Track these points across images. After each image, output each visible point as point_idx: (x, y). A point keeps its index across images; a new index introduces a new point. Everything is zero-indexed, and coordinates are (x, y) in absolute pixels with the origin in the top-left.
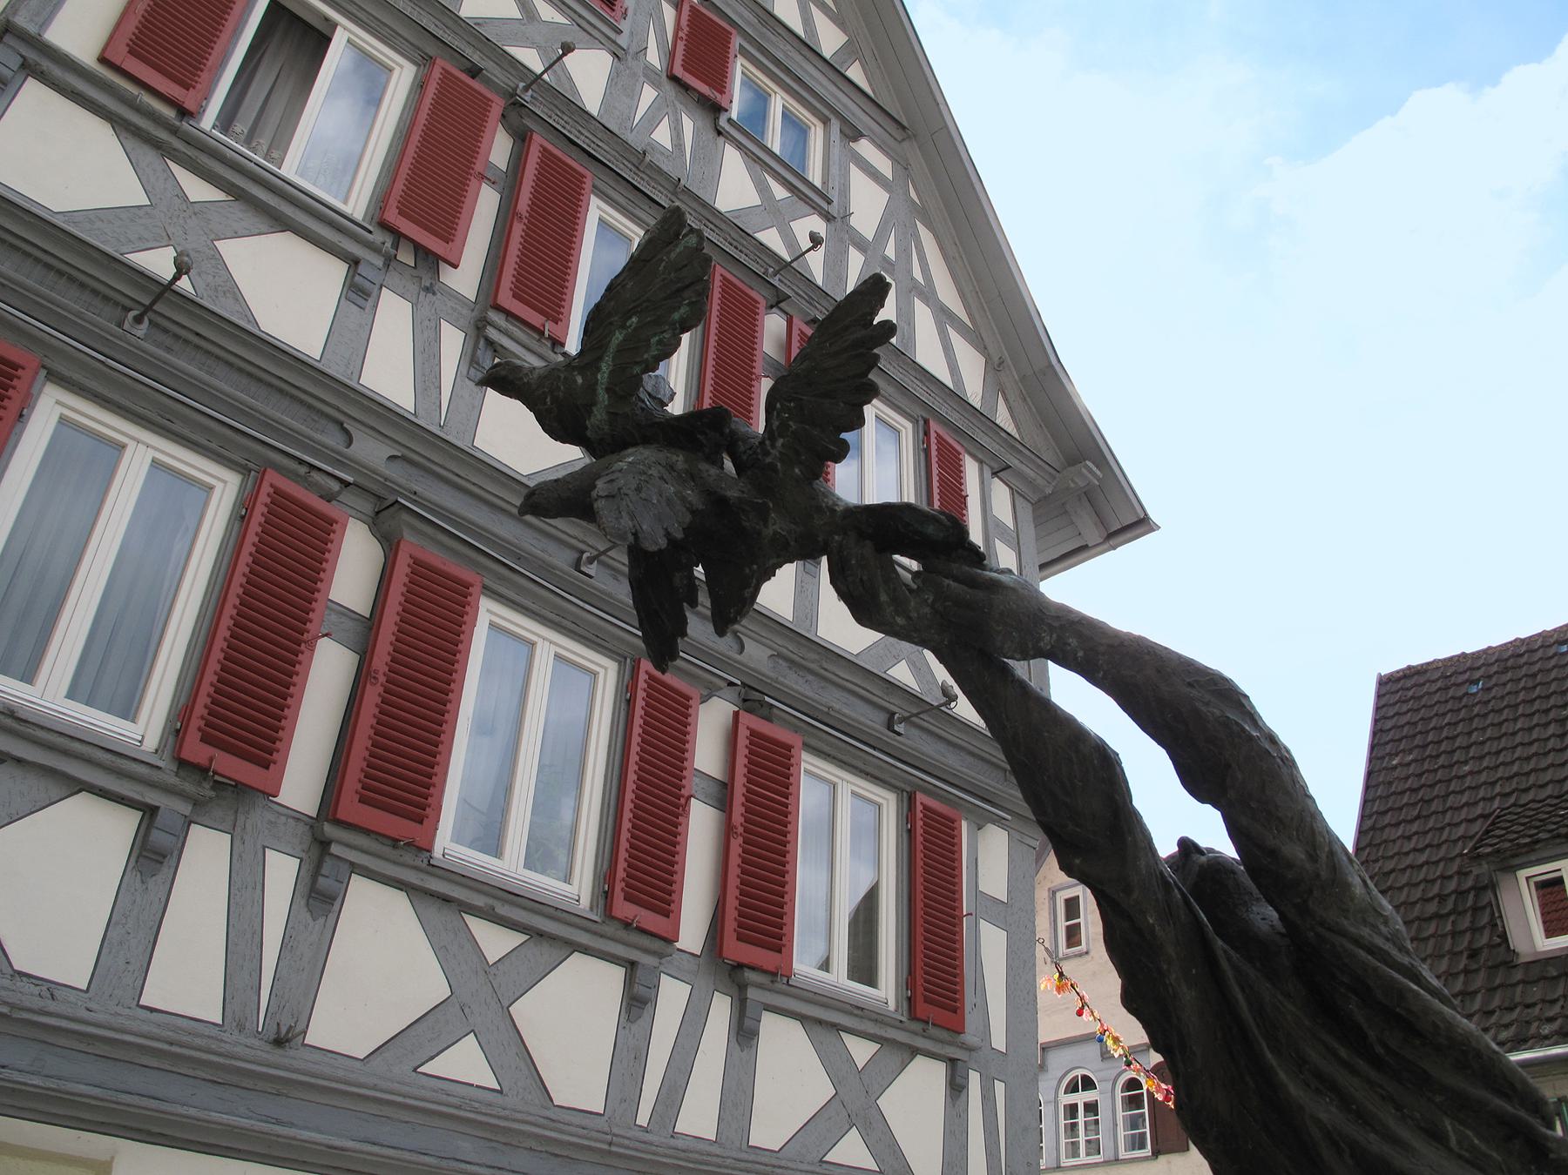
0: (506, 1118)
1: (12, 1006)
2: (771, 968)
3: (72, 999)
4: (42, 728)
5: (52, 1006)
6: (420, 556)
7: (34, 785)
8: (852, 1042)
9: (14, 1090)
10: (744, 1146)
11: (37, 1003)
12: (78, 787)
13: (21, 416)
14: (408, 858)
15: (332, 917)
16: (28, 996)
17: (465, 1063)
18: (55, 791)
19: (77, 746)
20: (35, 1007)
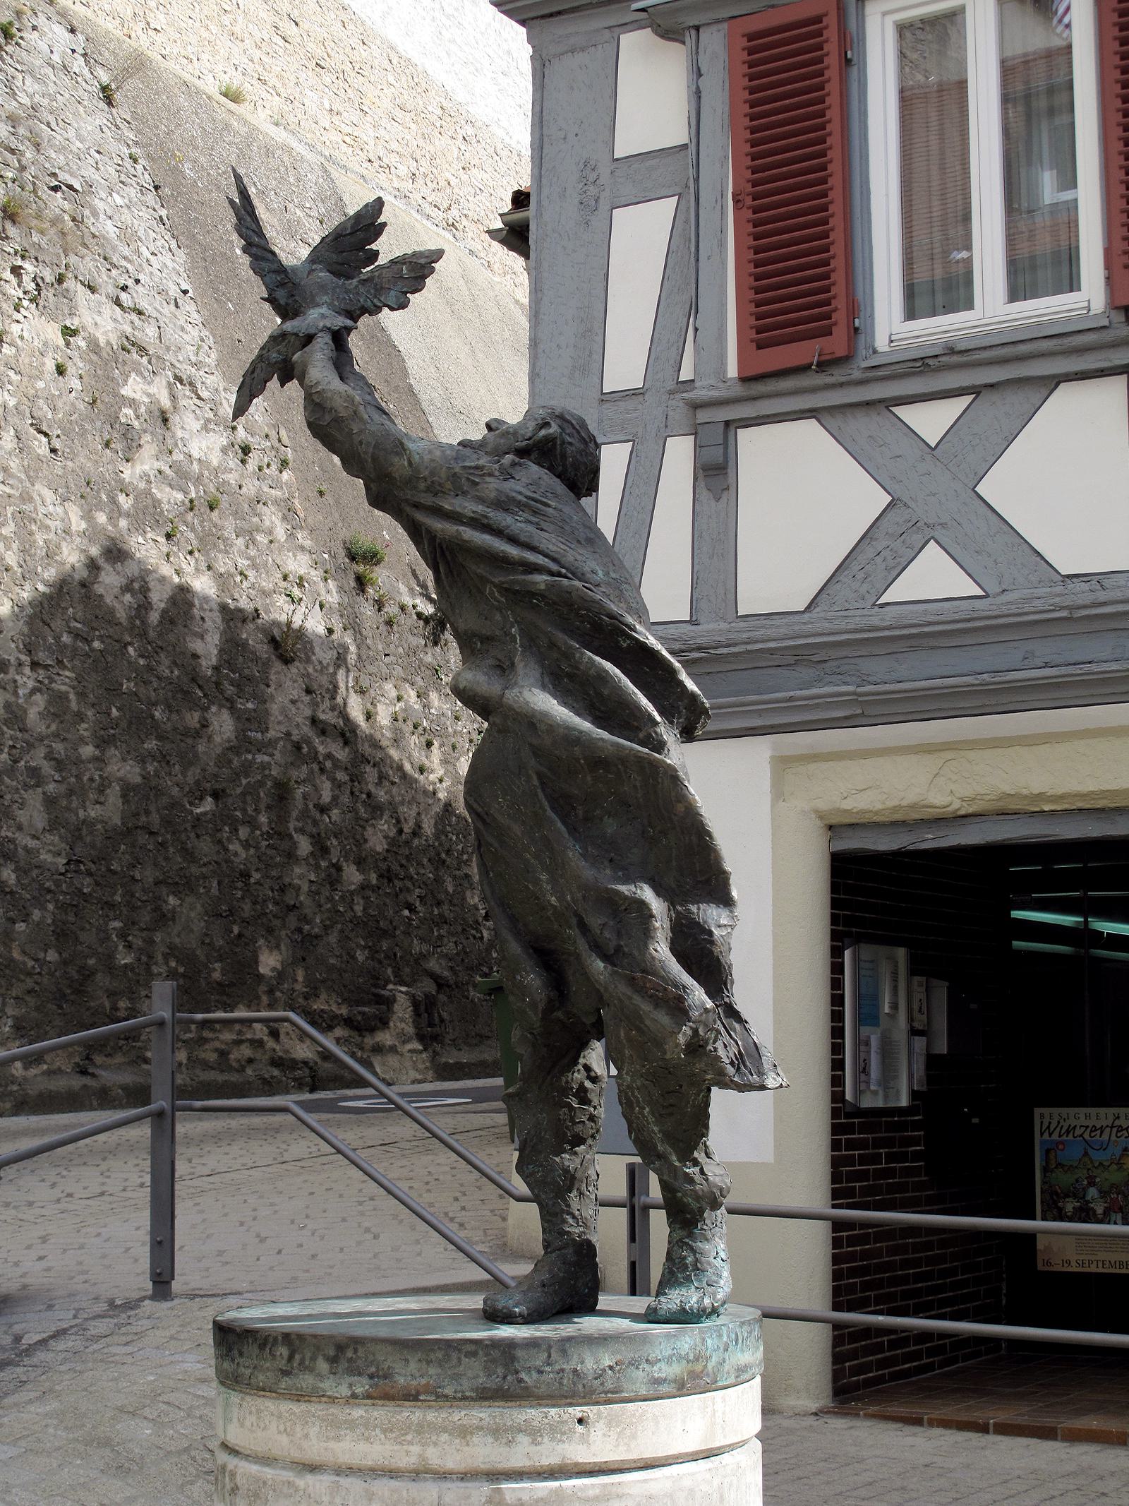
0: (968, 620)
1: (1071, 608)
2: (607, 405)
3: (1122, 582)
4: (985, 348)
5: (1102, 596)
6: (747, 31)
7: (1015, 400)
8: (912, 415)
9: (1103, 680)
10: (731, 616)
11: (1088, 599)
12: (1055, 382)
13: (848, 62)
14: (837, 375)
15: (732, 490)
16: (1081, 594)
17: (933, 578)
18: (1036, 398)
19: (1022, 348)
20: (1088, 602)
